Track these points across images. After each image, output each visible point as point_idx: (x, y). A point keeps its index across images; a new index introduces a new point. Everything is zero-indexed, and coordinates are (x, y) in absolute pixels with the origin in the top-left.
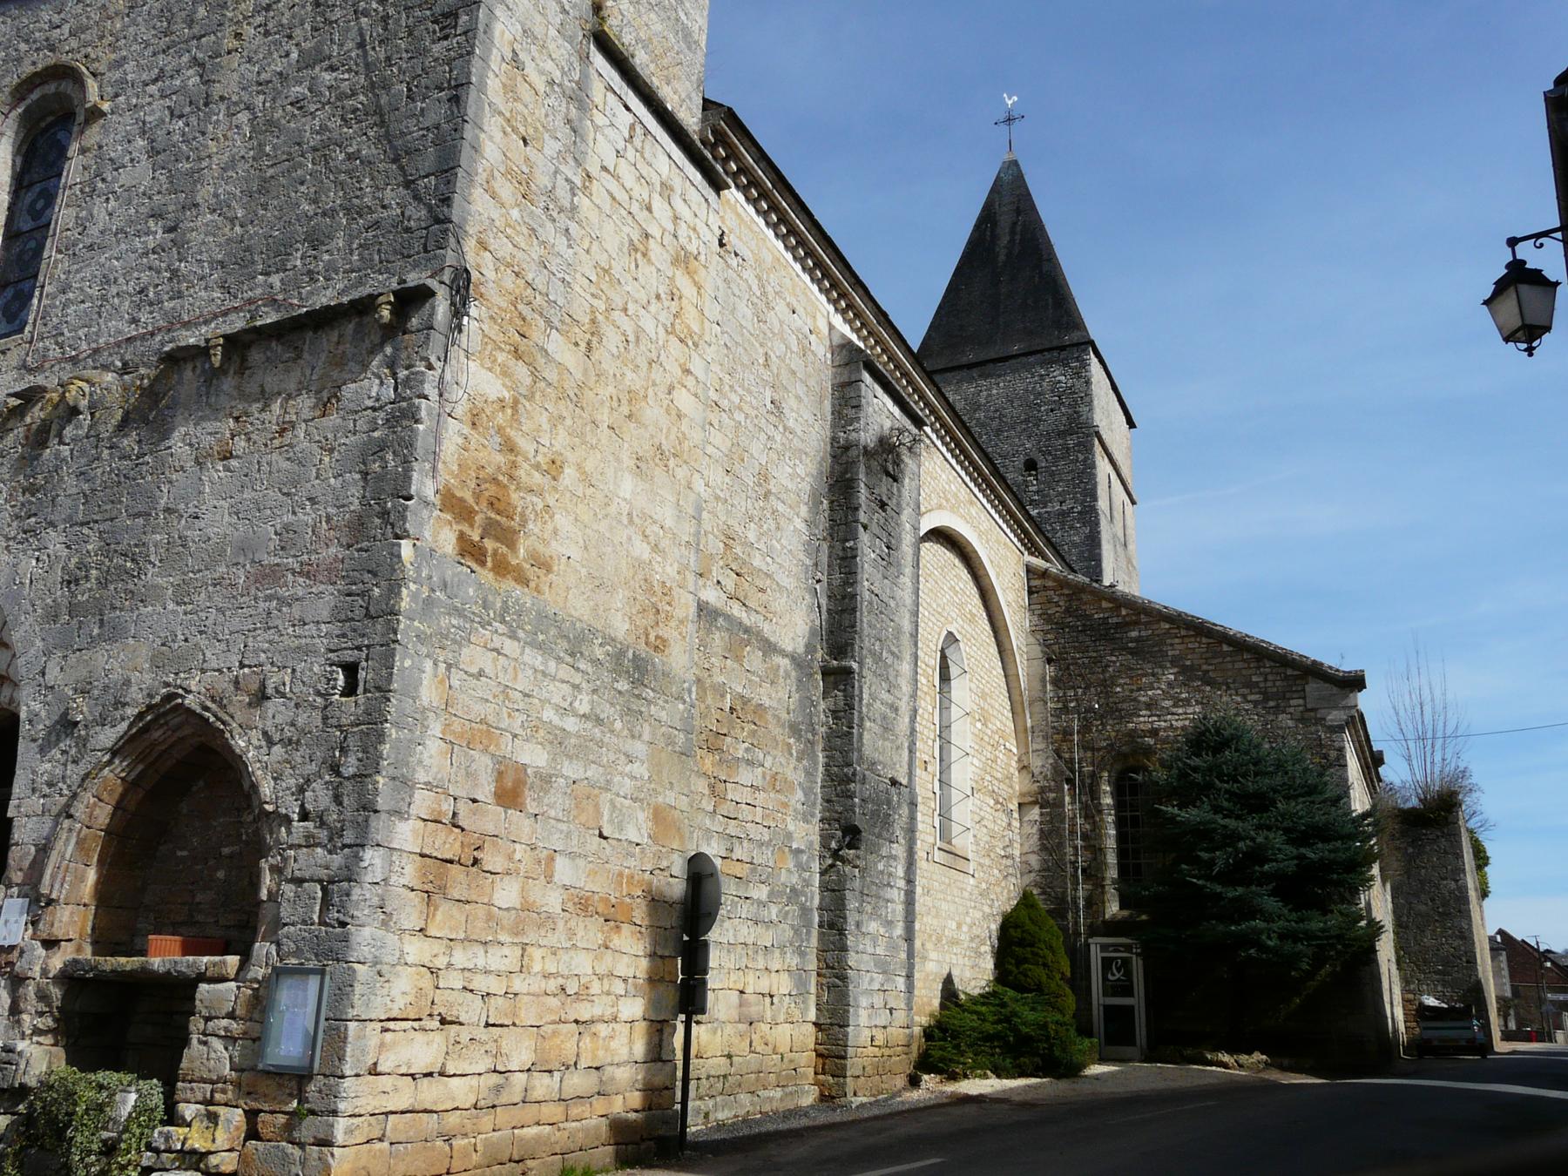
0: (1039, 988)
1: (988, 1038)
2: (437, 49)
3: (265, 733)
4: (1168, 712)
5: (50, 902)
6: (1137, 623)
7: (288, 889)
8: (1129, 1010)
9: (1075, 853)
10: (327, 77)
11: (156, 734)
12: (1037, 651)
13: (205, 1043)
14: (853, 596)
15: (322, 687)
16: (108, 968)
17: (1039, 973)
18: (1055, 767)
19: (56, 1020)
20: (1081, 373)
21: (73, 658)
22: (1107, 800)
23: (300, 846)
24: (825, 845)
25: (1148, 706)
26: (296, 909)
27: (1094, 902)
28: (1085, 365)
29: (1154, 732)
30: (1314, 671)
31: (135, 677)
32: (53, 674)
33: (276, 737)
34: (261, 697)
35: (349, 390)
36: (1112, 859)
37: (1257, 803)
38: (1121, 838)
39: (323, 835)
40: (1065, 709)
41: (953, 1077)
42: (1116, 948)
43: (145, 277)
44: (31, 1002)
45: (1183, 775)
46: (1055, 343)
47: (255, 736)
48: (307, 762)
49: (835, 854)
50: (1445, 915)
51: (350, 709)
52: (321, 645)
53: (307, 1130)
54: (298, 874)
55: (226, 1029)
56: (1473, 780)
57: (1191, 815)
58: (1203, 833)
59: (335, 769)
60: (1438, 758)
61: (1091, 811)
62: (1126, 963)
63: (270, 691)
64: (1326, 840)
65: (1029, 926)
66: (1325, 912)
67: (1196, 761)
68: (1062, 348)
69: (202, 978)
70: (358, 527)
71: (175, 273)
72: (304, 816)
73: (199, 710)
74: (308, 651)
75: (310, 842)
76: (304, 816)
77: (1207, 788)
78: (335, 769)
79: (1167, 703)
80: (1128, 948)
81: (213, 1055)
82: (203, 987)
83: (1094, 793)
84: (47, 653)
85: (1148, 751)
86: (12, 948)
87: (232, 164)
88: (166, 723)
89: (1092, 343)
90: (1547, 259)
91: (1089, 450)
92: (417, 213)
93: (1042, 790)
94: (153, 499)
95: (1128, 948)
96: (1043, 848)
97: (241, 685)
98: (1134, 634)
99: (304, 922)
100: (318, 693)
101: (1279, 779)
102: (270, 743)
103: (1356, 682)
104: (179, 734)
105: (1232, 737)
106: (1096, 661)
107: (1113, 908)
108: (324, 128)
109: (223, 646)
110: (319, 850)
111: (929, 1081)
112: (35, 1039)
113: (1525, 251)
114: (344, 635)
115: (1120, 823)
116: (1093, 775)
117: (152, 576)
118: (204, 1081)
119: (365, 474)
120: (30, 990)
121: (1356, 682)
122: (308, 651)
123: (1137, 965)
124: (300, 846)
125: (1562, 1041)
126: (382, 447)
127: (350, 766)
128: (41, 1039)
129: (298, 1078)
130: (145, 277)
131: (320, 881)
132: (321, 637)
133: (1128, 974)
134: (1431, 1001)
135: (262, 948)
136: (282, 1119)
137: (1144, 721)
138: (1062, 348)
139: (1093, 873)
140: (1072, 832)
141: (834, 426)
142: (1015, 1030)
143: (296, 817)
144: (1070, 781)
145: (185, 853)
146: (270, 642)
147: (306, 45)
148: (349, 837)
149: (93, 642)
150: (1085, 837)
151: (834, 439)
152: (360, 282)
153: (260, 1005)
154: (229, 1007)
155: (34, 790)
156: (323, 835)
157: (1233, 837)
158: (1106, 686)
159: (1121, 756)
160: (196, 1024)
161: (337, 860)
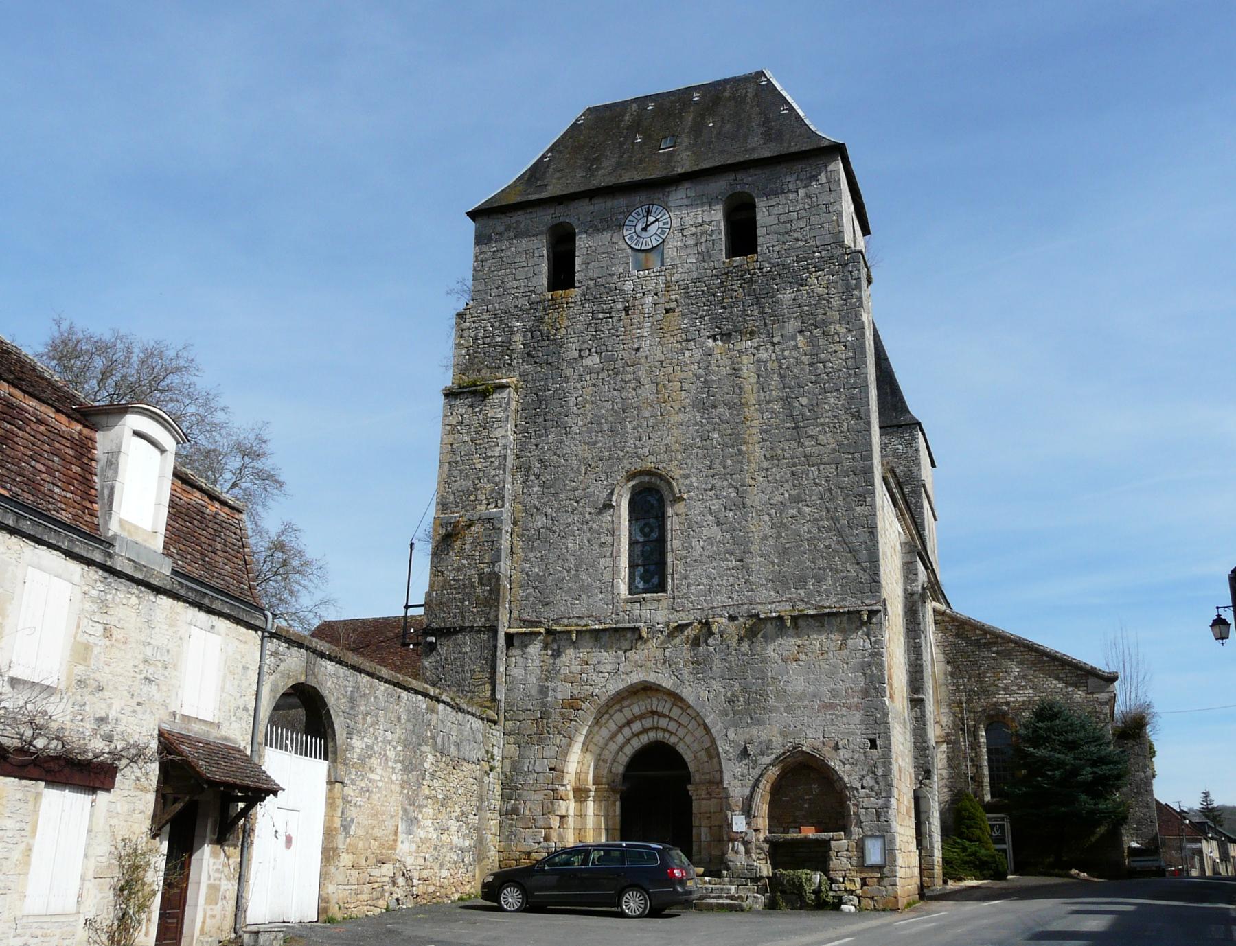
0: (979, 840)
1: (966, 863)
2: (858, 509)
4: (1018, 692)
6: (995, 643)
7: (863, 811)
8: (1004, 851)
9: (968, 768)
10: (806, 508)
12: (941, 657)
14: (921, 665)
17: (978, 832)
18: (954, 722)
20: (912, 443)
22: (983, 740)
24: (916, 778)
25: (1004, 689)
26: (868, 819)
27: (978, 794)
28: (914, 438)
29: (1007, 704)
30: (1092, 673)
32: (731, 736)
34: (836, 748)
35: (850, 642)
36: (986, 772)
37: (1072, 746)
38: (990, 761)
39: (873, 794)
40: (958, 690)
41: (960, 880)
42: (996, 819)
43: (731, 580)
45: (1035, 731)
46: (895, 422)
48: (860, 770)
49: (921, 782)
50: (1138, 793)
51: (875, 753)
52: (859, 732)
53: (886, 882)
56: (1154, 710)
57: (1042, 752)
58: (1045, 762)
59: (874, 773)
60: (1133, 696)
61: (975, 746)
62: (1002, 827)
64: (1106, 764)
65: (972, 810)
66: (1106, 799)
67: (1040, 724)
68: (900, 426)
69: (832, 839)
70: (865, 693)
71: (747, 581)
72: (863, 788)
74: (853, 733)
75: (868, 796)
76: (863, 788)
77: (1047, 739)
78: (874, 773)
79: (1014, 688)
80: (1002, 819)
82: (833, 843)
83: (976, 736)
84: (727, 728)
85: (1005, 714)
87: (765, 537)
89: (919, 424)
90: (1228, 616)
91: (919, 496)
92: (865, 577)
93: (948, 735)
94: (766, 674)
95: (1002, 819)
96: (950, 766)
98: (995, 649)
101: (1083, 734)
103: (1112, 679)
105: (1059, 712)
106: (975, 663)
107: (988, 798)
108: (809, 532)
111: (950, 882)
113: (1221, 611)
115: (989, 752)
116: (975, 726)
117: (772, 701)
119: (865, 674)
121: (1112, 679)
122: (853, 733)
123: (1008, 827)
126: (869, 664)
127: (880, 772)
129: (879, 868)
130: (731, 580)
132: (859, 729)
133: (1003, 832)
134: (1135, 845)
135: (855, 830)
137: (1001, 697)
138: (900, 426)
139: (977, 779)
140: (965, 758)
141: (905, 583)
142: (979, 859)
144: (962, 730)
147: (792, 492)
148: (884, 794)
149: (748, 725)
150: (972, 760)
151: (905, 590)
152: (843, 600)
153: (861, 847)
156: (873, 794)
157: (1061, 764)
158: (980, 677)
159: (990, 717)
160: (833, 854)
161: (881, 802)
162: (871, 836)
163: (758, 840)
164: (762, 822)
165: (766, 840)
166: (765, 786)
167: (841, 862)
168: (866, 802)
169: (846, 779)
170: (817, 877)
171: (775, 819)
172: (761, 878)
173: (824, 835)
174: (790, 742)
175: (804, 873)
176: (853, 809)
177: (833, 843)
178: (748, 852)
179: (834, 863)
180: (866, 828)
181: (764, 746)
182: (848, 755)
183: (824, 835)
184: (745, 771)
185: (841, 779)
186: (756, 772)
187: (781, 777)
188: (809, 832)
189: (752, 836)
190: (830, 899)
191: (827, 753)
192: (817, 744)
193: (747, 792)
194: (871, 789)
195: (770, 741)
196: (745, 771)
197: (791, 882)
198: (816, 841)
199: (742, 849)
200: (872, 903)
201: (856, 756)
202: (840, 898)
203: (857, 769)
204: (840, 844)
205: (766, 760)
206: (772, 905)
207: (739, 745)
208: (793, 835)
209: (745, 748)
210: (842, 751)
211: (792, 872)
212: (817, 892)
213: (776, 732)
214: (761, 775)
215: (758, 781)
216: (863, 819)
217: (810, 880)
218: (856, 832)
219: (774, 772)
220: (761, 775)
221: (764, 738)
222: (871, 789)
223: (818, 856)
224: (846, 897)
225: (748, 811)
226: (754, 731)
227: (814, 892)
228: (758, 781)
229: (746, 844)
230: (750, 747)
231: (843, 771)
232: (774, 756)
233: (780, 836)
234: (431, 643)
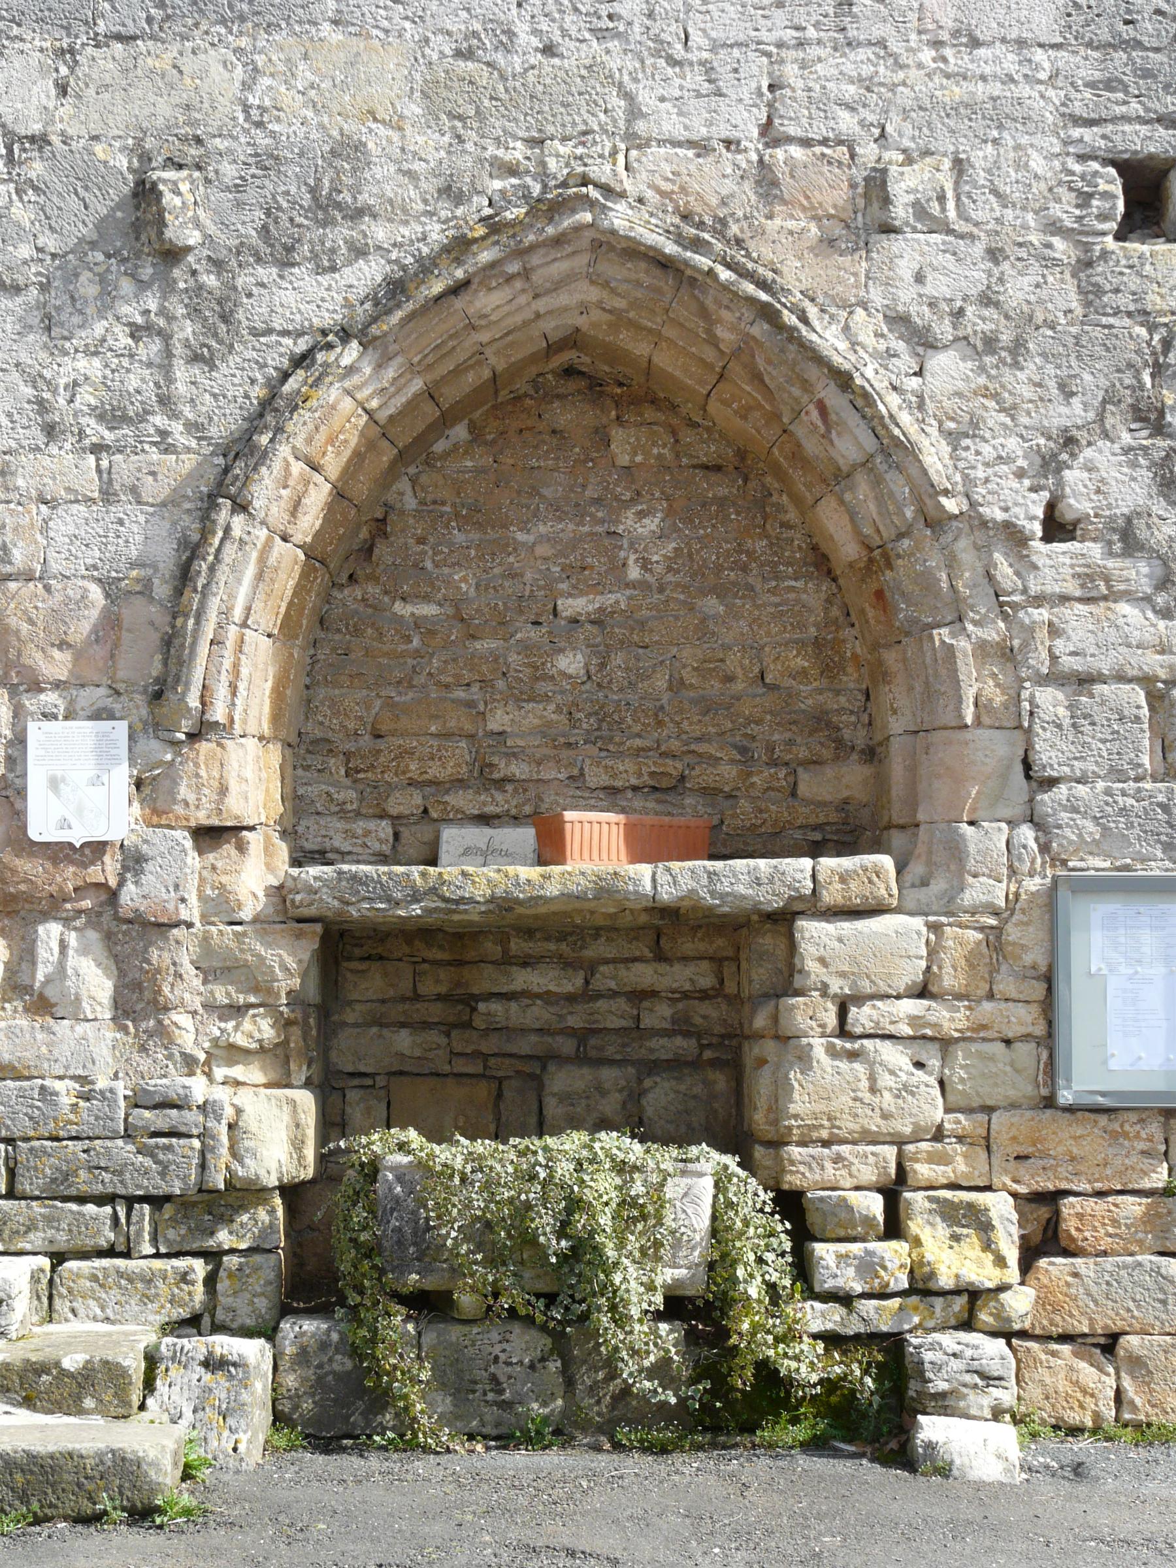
3: (899, 321)
5: (201, 731)
7: (1050, 701)
11: (487, 301)
13: (853, 1056)
15: (1064, 211)
16: (480, 892)
19: (284, 1025)
21: (102, 63)
23: (1065, 599)
31: (376, 139)
33: (944, 330)
34: (869, 215)
39: (1138, 573)
44: (186, 989)
47: (865, 325)
52: (1044, 104)
54: (1069, 663)
55: (914, 1020)
63: (900, 211)
69: (811, 905)
72: (1057, 527)
73: (671, 248)
74: (999, 117)
75: (1096, 590)
81: (885, 1080)
86: (98, 848)
88: (526, 274)
97: (788, 186)
99: (1118, 775)
100: (1054, 227)
102: (923, 341)
104: (541, 305)
109: (695, 79)
110: (1124, 608)
112: (220, 1073)
114: (1109, 84)
118: (874, 1139)
120: (179, 957)
122: (999, 117)
124: (1065, 599)
125: (3, 1024)
128: (238, 1072)
131: (1146, 681)
136: (1133, 1207)
143: (1037, 529)
145: (428, 610)
146: (868, 84)
154: (913, 972)
155: (51, 431)
156: (1138, 573)
160: (810, 1016)
162: (1125, 886)
163: (221, 906)
164: (249, 777)
165: (285, 911)
166: (292, 497)
167: (858, 1088)
168: (1081, 635)
169: (935, 457)
170: (696, 1187)
171: (339, 757)
172: (244, 1194)
173: (748, 879)
174: (497, 168)
175: (591, 1161)
176: (976, 685)
177: (816, 936)
178: (138, 1002)
179: (819, 1086)
180: (1073, 829)
181: (291, 186)
182: (956, 275)
183: (748, 879)
184: (138, 381)
185: (895, 451)
186: (221, 394)
187: (403, 447)
188: (598, 853)
189: (175, 879)
190: (806, 1366)
191: (788, 254)
192: (719, 183)
193: (138, 536)
194: (1127, 537)
195: (348, 151)
196: (138, 381)
197: (504, 1237)
198: (666, 924)
199: (94, 982)
200: (1099, 1380)
201: (1018, 289)
202: (892, 1356)
203: (1019, 383)
204: (868, 940)
205: (308, 298)
206: (337, 1415)
207: (86, 178)
208: (482, 870)
209: (145, 193)
210: (908, 252)
211: (502, 1157)
212: (699, 1312)
213: (388, 76)
214: (271, 409)
215: (240, 454)
216: (1050, 753)
217: (636, 1213)
218: (994, 856)
219: (345, 405)
220: (271, 409)
221: (297, 125)
222: (1127, 537)
223: (694, 1033)
224: (943, 1352)
225: (157, 703)
226: (211, 72)
227: (675, 1307)
228: (240, 454)
229: (132, 937)
230: (179, 194)
231: (923, 400)
232: (369, 274)
233: (391, 888)
234: (596, 1372)
